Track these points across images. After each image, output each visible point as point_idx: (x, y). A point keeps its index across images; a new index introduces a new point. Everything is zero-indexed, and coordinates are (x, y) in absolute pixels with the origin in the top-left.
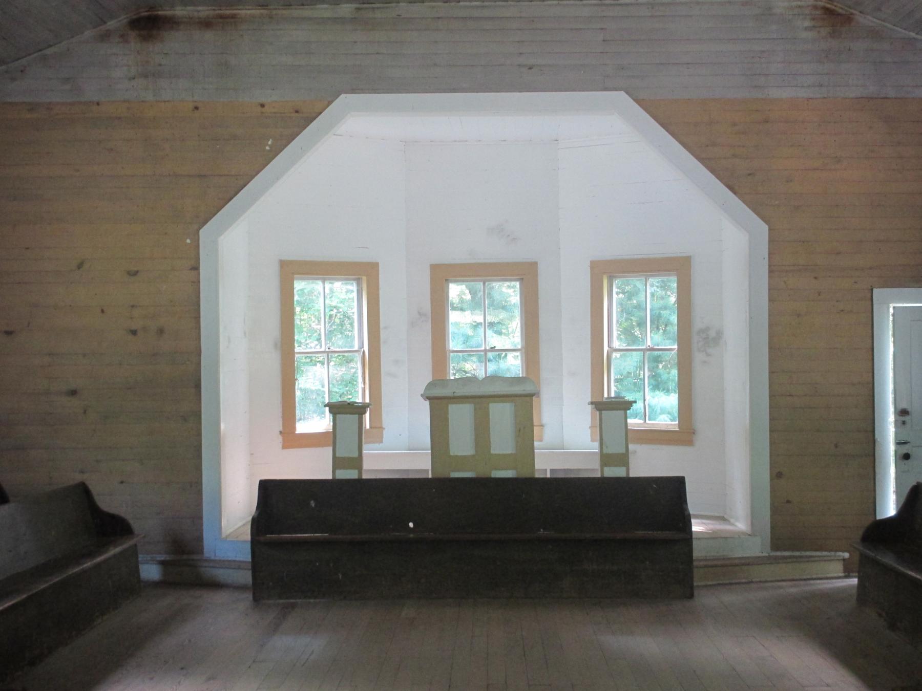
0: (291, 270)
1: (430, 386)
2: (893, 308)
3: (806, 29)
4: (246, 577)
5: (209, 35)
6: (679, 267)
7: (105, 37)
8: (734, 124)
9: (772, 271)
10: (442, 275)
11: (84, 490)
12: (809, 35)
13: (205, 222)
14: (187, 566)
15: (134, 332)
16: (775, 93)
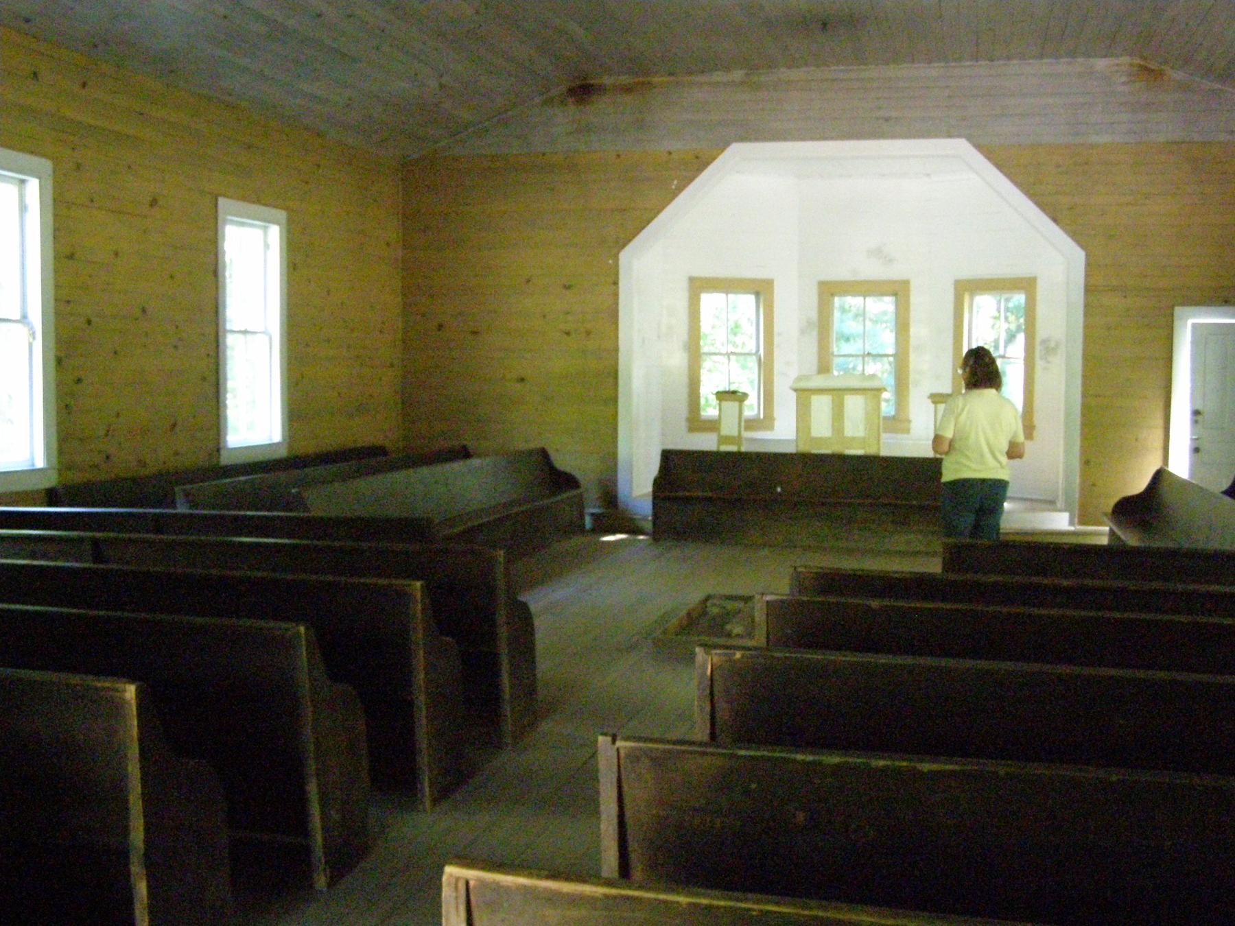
0: (698, 286)
1: (799, 379)
2: (1191, 325)
3: (1124, 83)
4: (648, 526)
5: (627, 98)
6: (1027, 285)
7: (549, 102)
8: (1058, 166)
9: (1089, 289)
10: (829, 291)
11: (544, 454)
12: (1125, 89)
13: (624, 246)
14: (613, 515)
15: (568, 334)
16: (1094, 139)
